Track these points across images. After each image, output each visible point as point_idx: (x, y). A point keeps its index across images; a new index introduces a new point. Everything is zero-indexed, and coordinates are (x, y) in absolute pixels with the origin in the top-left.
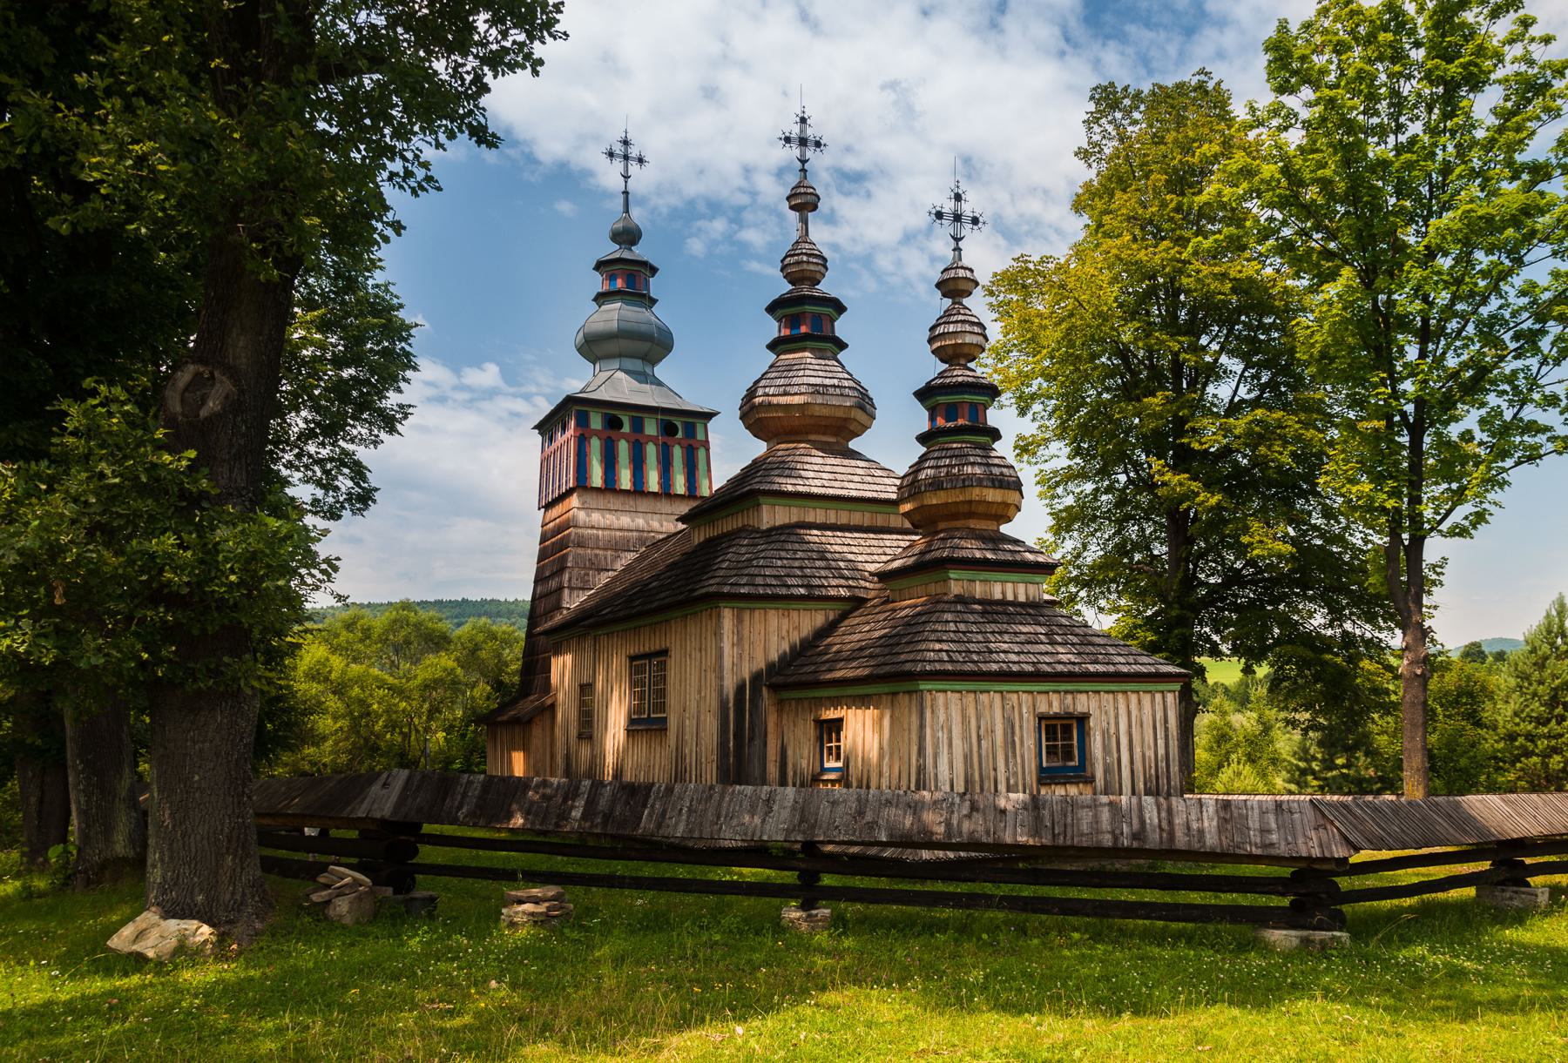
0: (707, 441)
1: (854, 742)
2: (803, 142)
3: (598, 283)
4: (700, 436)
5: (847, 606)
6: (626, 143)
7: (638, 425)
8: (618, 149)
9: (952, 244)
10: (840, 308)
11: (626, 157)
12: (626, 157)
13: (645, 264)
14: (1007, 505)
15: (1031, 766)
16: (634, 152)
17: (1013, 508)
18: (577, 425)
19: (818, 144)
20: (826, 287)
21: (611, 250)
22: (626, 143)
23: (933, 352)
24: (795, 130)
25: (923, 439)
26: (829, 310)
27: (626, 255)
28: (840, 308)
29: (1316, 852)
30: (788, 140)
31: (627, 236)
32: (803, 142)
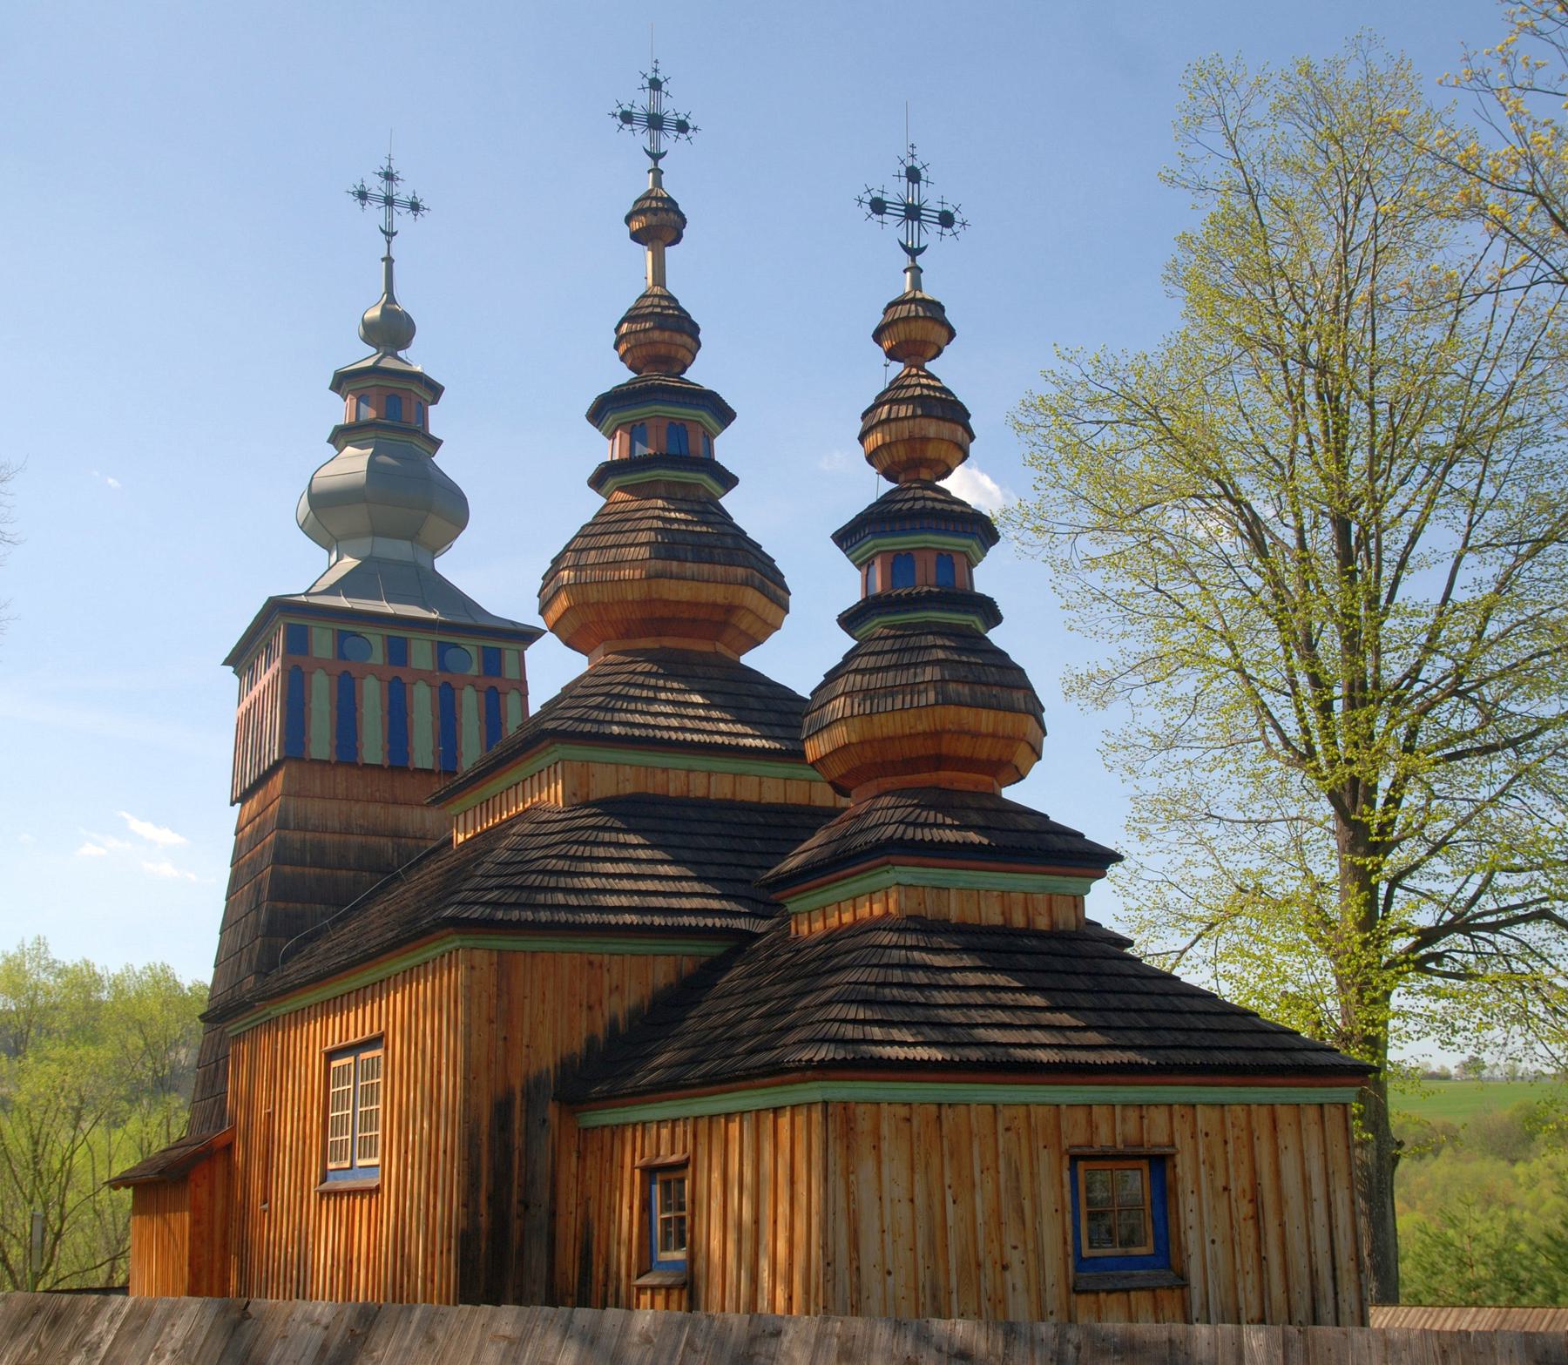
0: (523, 682)
1: (995, 1334)
2: (655, 122)
3: (340, 410)
4: (510, 672)
5: (715, 949)
6: (389, 176)
7: (398, 652)
8: (376, 186)
9: (906, 260)
10: (725, 415)
11: (389, 201)
12: (389, 201)
13: (419, 378)
14: (1012, 739)
15: (1054, 1268)
16: (402, 192)
17: (1023, 749)
18: (289, 650)
19: (682, 127)
20: (698, 374)
21: (362, 355)
22: (389, 176)
23: (870, 458)
24: (641, 102)
25: (849, 621)
26: (706, 417)
27: (389, 363)
28: (725, 415)
29: (858, 763)
30: (627, 117)
31: (391, 329)
32: (655, 122)
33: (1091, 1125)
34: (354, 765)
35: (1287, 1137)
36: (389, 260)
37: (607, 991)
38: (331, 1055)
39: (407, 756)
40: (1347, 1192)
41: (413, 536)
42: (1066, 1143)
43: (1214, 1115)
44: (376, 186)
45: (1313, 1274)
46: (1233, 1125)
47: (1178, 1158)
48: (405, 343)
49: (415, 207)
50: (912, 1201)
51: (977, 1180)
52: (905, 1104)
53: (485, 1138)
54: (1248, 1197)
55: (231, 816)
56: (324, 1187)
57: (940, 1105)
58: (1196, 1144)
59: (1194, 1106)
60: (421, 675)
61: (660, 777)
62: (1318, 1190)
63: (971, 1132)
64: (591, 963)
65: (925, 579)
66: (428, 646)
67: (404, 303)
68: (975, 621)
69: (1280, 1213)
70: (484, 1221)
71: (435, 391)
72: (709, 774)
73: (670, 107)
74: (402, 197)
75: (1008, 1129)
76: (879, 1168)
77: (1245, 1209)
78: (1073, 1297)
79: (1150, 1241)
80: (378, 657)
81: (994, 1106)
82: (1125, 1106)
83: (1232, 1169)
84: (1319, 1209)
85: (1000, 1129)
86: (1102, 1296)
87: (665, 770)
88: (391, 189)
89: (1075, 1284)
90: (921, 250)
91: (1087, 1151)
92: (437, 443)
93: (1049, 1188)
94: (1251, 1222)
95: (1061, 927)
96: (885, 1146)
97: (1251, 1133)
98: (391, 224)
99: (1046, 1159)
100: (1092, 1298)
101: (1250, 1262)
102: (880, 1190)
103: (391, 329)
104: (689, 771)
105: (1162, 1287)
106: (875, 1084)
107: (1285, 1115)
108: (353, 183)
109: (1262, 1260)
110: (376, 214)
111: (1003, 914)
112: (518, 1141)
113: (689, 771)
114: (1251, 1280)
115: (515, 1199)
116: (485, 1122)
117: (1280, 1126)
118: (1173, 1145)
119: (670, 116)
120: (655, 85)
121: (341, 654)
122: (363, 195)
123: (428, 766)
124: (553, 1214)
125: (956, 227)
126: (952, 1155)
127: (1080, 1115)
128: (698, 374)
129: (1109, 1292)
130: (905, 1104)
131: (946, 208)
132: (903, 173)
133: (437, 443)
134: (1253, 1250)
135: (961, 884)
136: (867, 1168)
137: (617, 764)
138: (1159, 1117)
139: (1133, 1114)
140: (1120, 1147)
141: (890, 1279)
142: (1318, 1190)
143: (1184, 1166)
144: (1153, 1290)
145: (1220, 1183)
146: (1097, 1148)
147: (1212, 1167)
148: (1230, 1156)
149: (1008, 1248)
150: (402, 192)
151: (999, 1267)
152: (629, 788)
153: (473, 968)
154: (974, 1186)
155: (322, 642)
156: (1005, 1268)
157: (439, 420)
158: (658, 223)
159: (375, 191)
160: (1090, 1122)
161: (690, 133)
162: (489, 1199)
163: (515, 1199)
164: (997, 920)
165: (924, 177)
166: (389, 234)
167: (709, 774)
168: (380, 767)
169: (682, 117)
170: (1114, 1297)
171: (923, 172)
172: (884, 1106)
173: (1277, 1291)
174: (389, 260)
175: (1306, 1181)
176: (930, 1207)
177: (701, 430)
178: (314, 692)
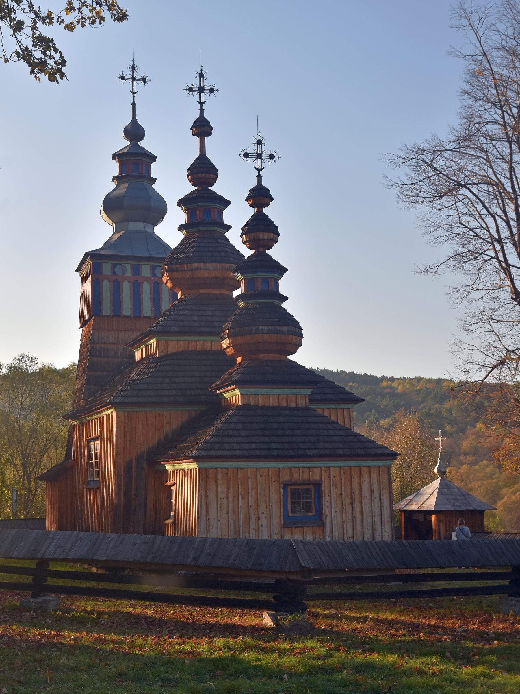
6: (133, 68)
7: (137, 270)
8: (128, 73)
9: (257, 173)
11: (134, 79)
12: (134, 79)
20: (217, 188)
24: (196, 83)
33: (292, 475)
34: (120, 316)
35: (365, 477)
36: (134, 104)
37: (165, 423)
38: (90, 441)
39: (141, 311)
40: (388, 495)
41: (145, 221)
42: (281, 480)
43: (338, 470)
44: (128, 73)
45: (373, 523)
46: (344, 473)
47: (323, 485)
48: (142, 137)
49: (144, 80)
50: (228, 498)
51: (250, 491)
52: (226, 469)
53: (123, 474)
54: (350, 497)
55: (79, 333)
56: (88, 487)
57: (238, 469)
58: (330, 480)
59: (330, 467)
60: (146, 279)
61: (193, 343)
62: (376, 494)
63: (248, 477)
64: (159, 414)
65: (260, 286)
66: (148, 267)
67: (140, 121)
68: (276, 302)
69: (361, 503)
70: (122, 501)
71: (153, 158)
72: (212, 342)
73: (207, 83)
74: (139, 77)
75: (261, 476)
76: (217, 488)
77: (348, 501)
78: (283, 529)
79: (314, 511)
80: (128, 273)
81: (257, 469)
82: (303, 468)
83: (343, 488)
84: (377, 501)
85: (258, 476)
86: (293, 529)
87: (196, 341)
88: (134, 73)
89: (284, 524)
90: (262, 169)
91: (289, 483)
92: (154, 180)
93: (275, 495)
94: (350, 505)
95: (300, 406)
96: (218, 482)
97: (351, 476)
98: (135, 89)
99: (274, 486)
100: (290, 529)
101: (349, 518)
102: (217, 495)
103: (134, 132)
104: (204, 341)
105: (315, 526)
106: (215, 463)
107: (365, 470)
108: (119, 74)
109: (353, 518)
110: (128, 85)
111: (278, 402)
112: (134, 475)
113: (204, 341)
114: (350, 524)
115: (133, 494)
116: (122, 471)
117: (362, 473)
118: (321, 480)
119: (207, 87)
120: (201, 75)
121: (114, 273)
122: (123, 78)
123: (149, 315)
124: (146, 499)
125: (275, 159)
126: (241, 484)
127: (288, 471)
128: (217, 188)
129: (296, 527)
130: (226, 469)
131: (272, 152)
132: (256, 142)
133: (154, 180)
134: (350, 514)
135: (263, 393)
136: (212, 488)
137: (178, 341)
138: (317, 471)
139: (307, 470)
140: (301, 481)
141: (219, 522)
142: (376, 494)
143: (325, 487)
144: (312, 527)
145: (339, 492)
146: (293, 481)
147: (336, 487)
148: (343, 483)
149: (260, 513)
150: (139, 74)
151: (257, 519)
152: (182, 349)
153: (119, 418)
154: (249, 493)
155: (107, 269)
156: (259, 519)
157: (155, 170)
158: (202, 128)
159: (128, 75)
160: (291, 473)
161: (215, 92)
162: (124, 494)
163: (133, 494)
164: (276, 404)
165: (263, 142)
166: (134, 93)
167: (212, 342)
168: (130, 317)
169: (212, 87)
170: (298, 529)
171: (243, 158)
172: (219, 469)
173: (359, 528)
174: (134, 104)
175: (372, 491)
176: (234, 500)
177: (216, 210)
178: (104, 289)
